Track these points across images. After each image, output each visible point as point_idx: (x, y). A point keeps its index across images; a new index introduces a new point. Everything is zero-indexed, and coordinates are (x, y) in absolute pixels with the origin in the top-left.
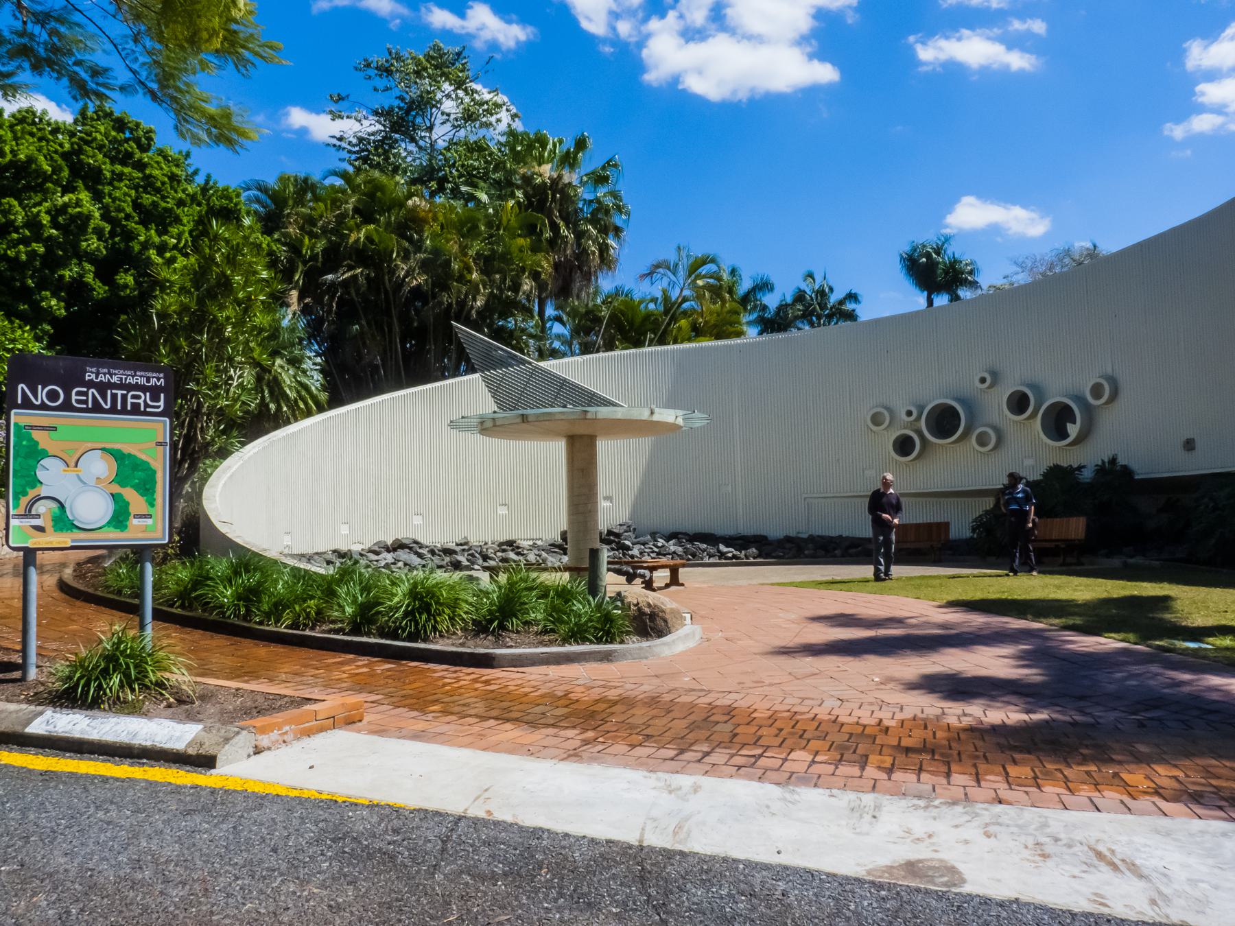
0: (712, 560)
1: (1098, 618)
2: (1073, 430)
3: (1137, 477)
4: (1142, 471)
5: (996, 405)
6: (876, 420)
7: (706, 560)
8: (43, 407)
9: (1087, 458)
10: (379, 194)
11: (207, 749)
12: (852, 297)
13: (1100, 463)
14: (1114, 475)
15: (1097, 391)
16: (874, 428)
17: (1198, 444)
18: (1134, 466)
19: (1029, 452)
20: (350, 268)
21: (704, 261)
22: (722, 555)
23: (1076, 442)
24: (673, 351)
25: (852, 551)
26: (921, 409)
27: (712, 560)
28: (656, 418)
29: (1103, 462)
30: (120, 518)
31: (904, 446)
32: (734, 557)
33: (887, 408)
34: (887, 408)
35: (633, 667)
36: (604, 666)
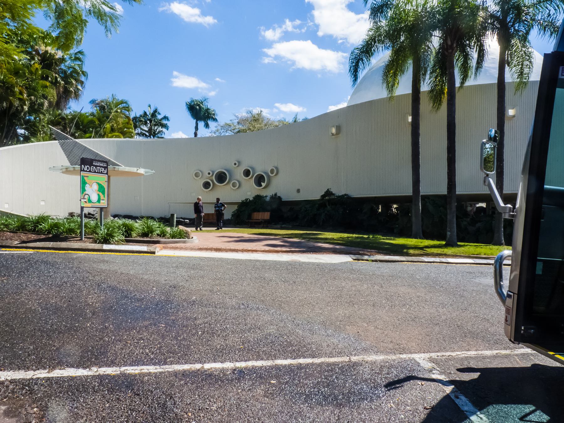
1: (296, 236)
2: (264, 185)
4: (284, 199)
5: (239, 174)
6: (197, 175)
8: (86, 171)
9: (268, 193)
11: (154, 251)
12: (166, 118)
15: (272, 171)
17: (301, 191)
19: (248, 190)
21: (122, 102)
23: (264, 188)
24: (117, 141)
26: (213, 172)
28: (139, 172)
30: (99, 201)
31: (206, 185)
33: (200, 171)
34: (200, 171)
35: (187, 245)
36: (185, 244)
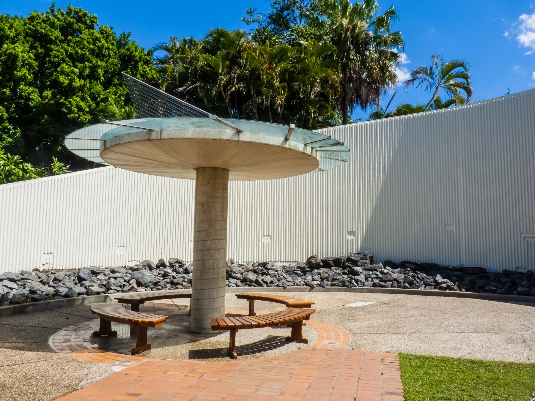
0: (428, 289)
7: (422, 289)
10: (222, 39)
20: (193, 83)
21: (454, 66)
22: (437, 285)
27: (428, 289)
32: (448, 287)
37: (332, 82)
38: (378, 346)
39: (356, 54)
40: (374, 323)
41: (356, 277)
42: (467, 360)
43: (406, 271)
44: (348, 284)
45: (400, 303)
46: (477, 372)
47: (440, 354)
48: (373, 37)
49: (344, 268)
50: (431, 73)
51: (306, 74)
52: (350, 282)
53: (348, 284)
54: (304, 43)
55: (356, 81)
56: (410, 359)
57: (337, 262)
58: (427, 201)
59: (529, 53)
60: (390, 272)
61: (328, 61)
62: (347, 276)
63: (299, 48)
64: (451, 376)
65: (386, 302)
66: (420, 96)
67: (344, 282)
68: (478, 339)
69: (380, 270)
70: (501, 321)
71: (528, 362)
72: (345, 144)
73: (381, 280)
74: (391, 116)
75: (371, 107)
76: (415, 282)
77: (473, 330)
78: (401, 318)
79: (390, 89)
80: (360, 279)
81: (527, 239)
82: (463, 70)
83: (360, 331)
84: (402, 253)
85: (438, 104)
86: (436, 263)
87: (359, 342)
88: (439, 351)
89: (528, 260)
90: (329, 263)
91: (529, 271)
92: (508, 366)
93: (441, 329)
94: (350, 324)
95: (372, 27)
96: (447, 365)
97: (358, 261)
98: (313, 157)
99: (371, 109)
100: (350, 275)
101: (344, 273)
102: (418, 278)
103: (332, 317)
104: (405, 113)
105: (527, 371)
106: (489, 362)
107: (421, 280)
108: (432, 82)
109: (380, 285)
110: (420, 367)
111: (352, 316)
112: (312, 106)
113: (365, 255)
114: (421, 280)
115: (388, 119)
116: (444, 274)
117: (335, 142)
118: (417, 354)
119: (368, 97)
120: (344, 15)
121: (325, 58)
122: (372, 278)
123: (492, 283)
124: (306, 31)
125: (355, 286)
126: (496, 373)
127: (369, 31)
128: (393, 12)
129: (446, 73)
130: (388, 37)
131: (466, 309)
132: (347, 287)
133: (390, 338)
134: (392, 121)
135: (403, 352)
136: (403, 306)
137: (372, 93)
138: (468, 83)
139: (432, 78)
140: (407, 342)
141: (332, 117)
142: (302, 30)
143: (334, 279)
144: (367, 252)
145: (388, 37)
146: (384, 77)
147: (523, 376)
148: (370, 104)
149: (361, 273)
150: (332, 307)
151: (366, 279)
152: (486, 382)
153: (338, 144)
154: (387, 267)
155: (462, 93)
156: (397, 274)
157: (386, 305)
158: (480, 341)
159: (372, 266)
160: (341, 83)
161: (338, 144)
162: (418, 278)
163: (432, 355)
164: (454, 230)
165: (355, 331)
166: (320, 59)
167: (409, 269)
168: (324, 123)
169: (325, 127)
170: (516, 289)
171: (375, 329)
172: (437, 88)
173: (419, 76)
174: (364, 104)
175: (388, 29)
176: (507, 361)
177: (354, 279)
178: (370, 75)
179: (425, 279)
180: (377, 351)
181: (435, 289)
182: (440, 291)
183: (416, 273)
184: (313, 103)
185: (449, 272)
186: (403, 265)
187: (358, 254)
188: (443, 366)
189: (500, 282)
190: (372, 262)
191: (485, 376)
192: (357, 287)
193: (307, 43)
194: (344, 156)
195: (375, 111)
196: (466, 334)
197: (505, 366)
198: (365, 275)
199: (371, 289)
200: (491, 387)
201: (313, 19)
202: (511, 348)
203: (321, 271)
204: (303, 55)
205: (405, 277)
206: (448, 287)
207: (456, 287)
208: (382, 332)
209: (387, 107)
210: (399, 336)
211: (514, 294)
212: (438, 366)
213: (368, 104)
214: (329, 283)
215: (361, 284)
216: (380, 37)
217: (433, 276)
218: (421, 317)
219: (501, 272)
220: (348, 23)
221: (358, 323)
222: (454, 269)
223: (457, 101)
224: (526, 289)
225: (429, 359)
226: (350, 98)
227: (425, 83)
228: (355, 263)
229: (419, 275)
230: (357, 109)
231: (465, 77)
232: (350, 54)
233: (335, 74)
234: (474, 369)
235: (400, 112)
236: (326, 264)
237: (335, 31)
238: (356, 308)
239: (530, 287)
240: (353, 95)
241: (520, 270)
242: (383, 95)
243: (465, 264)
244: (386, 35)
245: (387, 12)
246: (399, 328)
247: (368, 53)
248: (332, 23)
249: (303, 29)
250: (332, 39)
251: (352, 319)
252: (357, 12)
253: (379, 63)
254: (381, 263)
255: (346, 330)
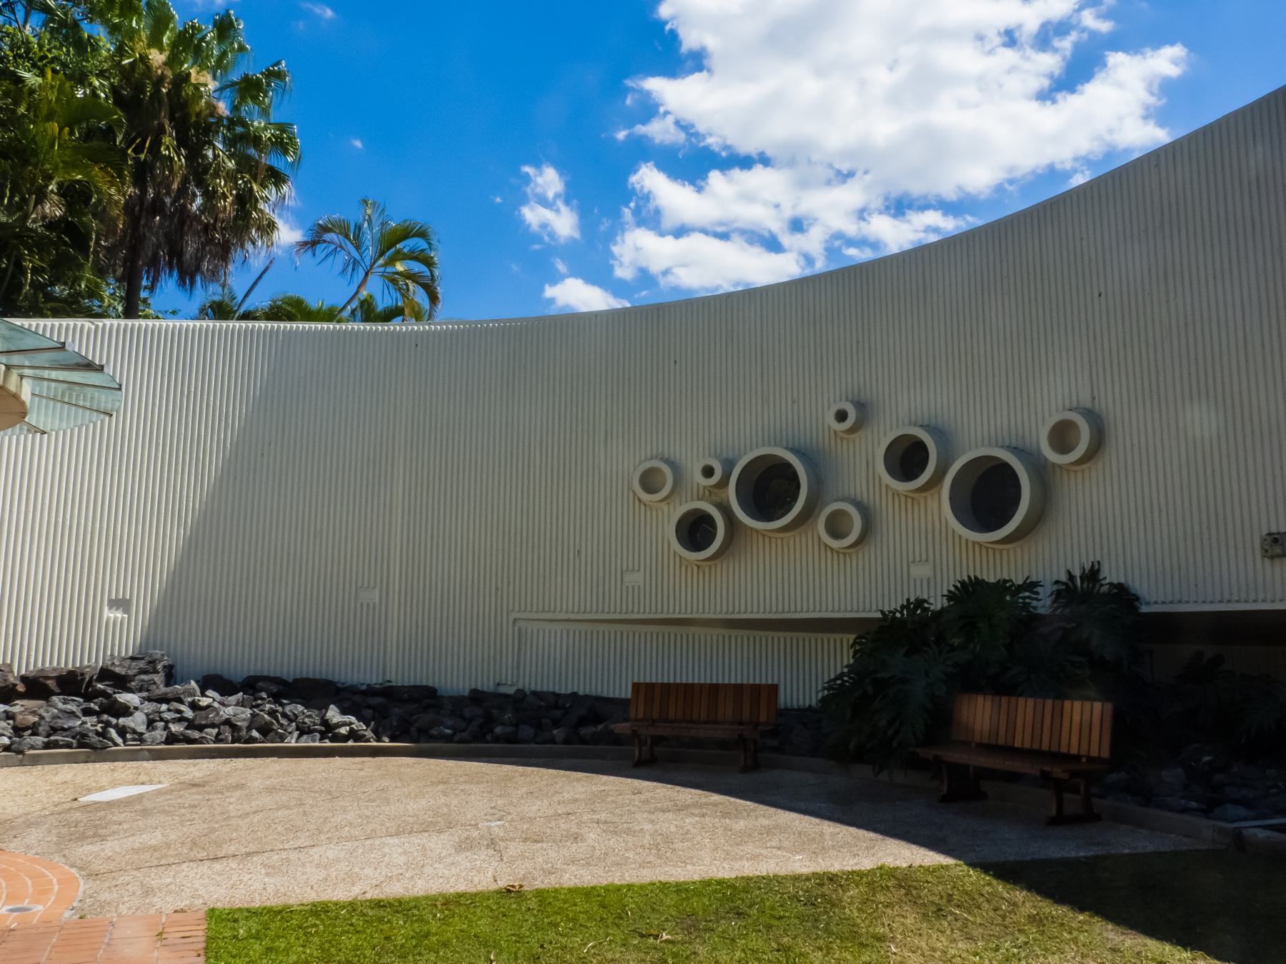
0: (306, 742)
3: (1144, 609)
4: (1157, 595)
5: (863, 467)
6: (649, 482)
7: (292, 742)
9: (1039, 561)
13: (1064, 578)
14: (1094, 597)
15: (1062, 436)
16: (646, 497)
18: (1139, 586)
19: (923, 554)
21: (406, 234)
22: (328, 730)
25: (586, 731)
26: (729, 465)
27: (306, 742)
29: (1071, 577)
31: (695, 531)
32: (353, 735)
37: (99, 201)
38: (156, 899)
39: (179, 147)
40: (155, 838)
41: (122, 721)
42: (370, 901)
43: (256, 699)
44: (95, 739)
45: (232, 781)
46: (386, 927)
47: (312, 897)
48: (227, 118)
49: (88, 697)
50: (357, 237)
51: (26, 162)
52: (103, 734)
53: (95, 739)
54: (31, 78)
55: (173, 215)
56: (236, 921)
57: (71, 683)
58: (321, 531)
59: (537, 247)
60: (216, 705)
61: (96, 142)
62: (94, 719)
63: (12, 87)
64: (327, 946)
65: (197, 781)
66: (326, 283)
67: (84, 736)
68: (400, 850)
69: (190, 699)
70: (455, 802)
71: (494, 887)
72: (109, 370)
73: (191, 725)
74: (255, 319)
75: (205, 287)
76: (276, 726)
77: (392, 830)
78: (228, 818)
79: (255, 254)
80: (132, 725)
81: (521, 624)
82: (425, 246)
83: (111, 866)
84: (289, 655)
85: (368, 312)
86: (330, 678)
87: (105, 896)
88: (308, 889)
89: (518, 668)
90: (46, 686)
91: (518, 691)
92: (452, 904)
93: (323, 837)
94: (85, 850)
95: (227, 92)
96: (322, 920)
97: (132, 678)
98: (7, 391)
99: (206, 293)
100: (105, 717)
101: (87, 712)
102: (284, 715)
103: (33, 836)
104: (290, 318)
105: (488, 907)
106: (416, 899)
107: (291, 721)
108: (358, 257)
109: (183, 742)
110: (257, 937)
111: (96, 827)
112: (31, 252)
113: (153, 662)
114: (291, 721)
115: (243, 324)
116: (346, 705)
117: (80, 360)
118: (256, 904)
119: (199, 260)
120: (155, 41)
121: (88, 136)
122: (167, 722)
123: (445, 720)
124: (41, 47)
125: (116, 745)
126: (428, 922)
127: (218, 99)
128: (279, 75)
129: (390, 242)
130: (265, 129)
131: (385, 783)
132: (91, 748)
133: (192, 874)
134: (252, 331)
135: (219, 905)
136: (241, 786)
137: (210, 251)
138: (432, 276)
139: (358, 248)
140: (234, 878)
141: (93, 293)
142: (28, 42)
143: (54, 730)
144: (158, 653)
145: (265, 129)
146: (245, 221)
147: (479, 919)
148: (204, 280)
149: (136, 708)
150: (38, 807)
151: (150, 724)
152: (402, 946)
153: (89, 366)
154: (210, 693)
155: (420, 297)
156: (233, 709)
157: (194, 790)
158: (405, 853)
159: (168, 689)
160: (128, 208)
161: (89, 366)
162: (284, 715)
163: (291, 902)
164: (377, 600)
165: (95, 867)
166: (71, 133)
167: (264, 695)
168: (70, 304)
169: (69, 316)
170: (492, 731)
171: (156, 855)
172: (367, 274)
173: (328, 236)
174: (187, 276)
175: (265, 112)
176: (452, 891)
177: (116, 727)
178: (209, 207)
179: (300, 718)
180: (152, 911)
181: (321, 739)
182: (335, 744)
183: (282, 705)
184: (40, 245)
185: (358, 698)
186: (250, 686)
187: (133, 659)
188: (315, 925)
189: (463, 718)
190: (170, 678)
191: (402, 930)
192: (122, 747)
193: (40, 80)
194: (104, 399)
195: (217, 298)
196: (377, 842)
197: (446, 903)
198: (147, 715)
199: (160, 750)
200: (410, 958)
201: (63, 24)
202: (464, 860)
203: (16, 709)
204: (22, 110)
205: (253, 715)
206: (353, 735)
207: (369, 734)
208: (171, 860)
209: (247, 295)
210: (217, 866)
211: (487, 742)
212: (300, 927)
213: (198, 278)
214: (39, 740)
215: (134, 740)
216: (243, 124)
217: (320, 709)
218: (280, 813)
219: (466, 694)
220: (165, 64)
221: (109, 844)
222: (371, 691)
223: (406, 311)
224: (510, 729)
225: (281, 913)
226: (150, 254)
227: (342, 257)
228: (122, 682)
229: (287, 709)
230: (169, 285)
231: (429, 263)
232: (160, 144)
233: (112, 184)
234: (380, 920)
235: (275, 314)
236: (36, 687)
237: (127, 73)
238: (110, 804)
239: (516, 725)
240: (159, 246)
241: (502, 690)
242: (238, 264)
243: (393, 679)
244: (258, 123)
245: (268, 70)
246: (219, 845)
247: (210, 154)
248: (120, 51)
249: (35, 40)
250: (114, 90)
251: (94, 836)
252: (188, 43)
253: (236, 183)
254: (193, 683)
255: (72, 866)
